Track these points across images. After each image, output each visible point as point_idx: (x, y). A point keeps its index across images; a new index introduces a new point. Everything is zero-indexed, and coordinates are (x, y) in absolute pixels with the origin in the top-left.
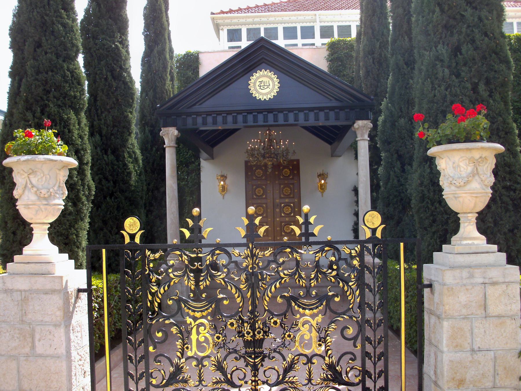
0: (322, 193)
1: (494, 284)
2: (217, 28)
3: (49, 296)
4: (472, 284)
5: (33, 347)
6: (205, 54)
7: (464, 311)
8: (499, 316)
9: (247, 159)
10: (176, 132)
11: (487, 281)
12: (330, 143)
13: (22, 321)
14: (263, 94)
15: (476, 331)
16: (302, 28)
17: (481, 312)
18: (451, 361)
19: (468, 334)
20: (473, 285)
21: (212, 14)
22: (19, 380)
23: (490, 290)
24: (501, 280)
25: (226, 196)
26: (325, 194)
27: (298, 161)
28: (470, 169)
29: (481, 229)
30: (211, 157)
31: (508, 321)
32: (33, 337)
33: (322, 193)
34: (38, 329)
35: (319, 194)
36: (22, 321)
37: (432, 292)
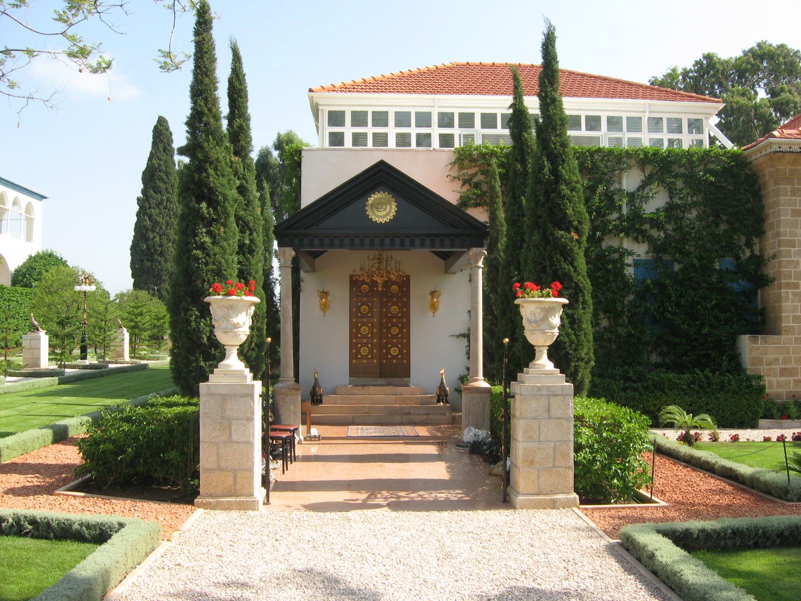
0: (434, 313)
1: (555, 395)
2: (316, 110)
3: (244, 399)
4: (540, 395)
5: (230, 436)
6: (533, 492)
7: (534, 414)
8: (558, 418)
9: (352, 273)
10: (293, 253)
11: (550, 393)
12: (445, 259)
13: (223, 417)
14: (380, 217)
15: (542, 428)
16: (417, 113)
17: (546, 415)
18: (524, 449)
19: (537, 429)
20: (541, 396)
21: (311, 90)
22: (218, 460)
23: (553, 400)
24: (560, 393)
25: (327, 313)
26: (436, 314)
27: (408, 277)
28: (542, 315)
29: (550, 357)
30: (313, 270)
31: (564, 422)
32: (230, 428)
33: (434, 313)
34: (234, 422)
35: (431, 314)
36: (223, 417)
37: (515, 401)
